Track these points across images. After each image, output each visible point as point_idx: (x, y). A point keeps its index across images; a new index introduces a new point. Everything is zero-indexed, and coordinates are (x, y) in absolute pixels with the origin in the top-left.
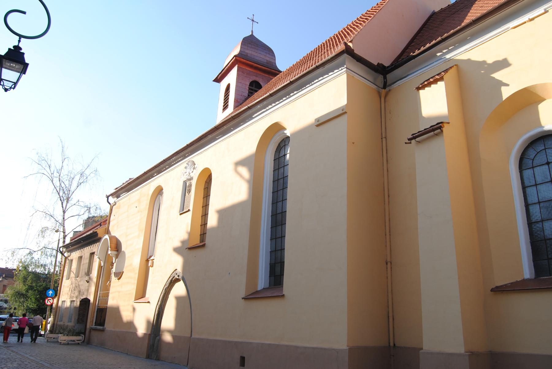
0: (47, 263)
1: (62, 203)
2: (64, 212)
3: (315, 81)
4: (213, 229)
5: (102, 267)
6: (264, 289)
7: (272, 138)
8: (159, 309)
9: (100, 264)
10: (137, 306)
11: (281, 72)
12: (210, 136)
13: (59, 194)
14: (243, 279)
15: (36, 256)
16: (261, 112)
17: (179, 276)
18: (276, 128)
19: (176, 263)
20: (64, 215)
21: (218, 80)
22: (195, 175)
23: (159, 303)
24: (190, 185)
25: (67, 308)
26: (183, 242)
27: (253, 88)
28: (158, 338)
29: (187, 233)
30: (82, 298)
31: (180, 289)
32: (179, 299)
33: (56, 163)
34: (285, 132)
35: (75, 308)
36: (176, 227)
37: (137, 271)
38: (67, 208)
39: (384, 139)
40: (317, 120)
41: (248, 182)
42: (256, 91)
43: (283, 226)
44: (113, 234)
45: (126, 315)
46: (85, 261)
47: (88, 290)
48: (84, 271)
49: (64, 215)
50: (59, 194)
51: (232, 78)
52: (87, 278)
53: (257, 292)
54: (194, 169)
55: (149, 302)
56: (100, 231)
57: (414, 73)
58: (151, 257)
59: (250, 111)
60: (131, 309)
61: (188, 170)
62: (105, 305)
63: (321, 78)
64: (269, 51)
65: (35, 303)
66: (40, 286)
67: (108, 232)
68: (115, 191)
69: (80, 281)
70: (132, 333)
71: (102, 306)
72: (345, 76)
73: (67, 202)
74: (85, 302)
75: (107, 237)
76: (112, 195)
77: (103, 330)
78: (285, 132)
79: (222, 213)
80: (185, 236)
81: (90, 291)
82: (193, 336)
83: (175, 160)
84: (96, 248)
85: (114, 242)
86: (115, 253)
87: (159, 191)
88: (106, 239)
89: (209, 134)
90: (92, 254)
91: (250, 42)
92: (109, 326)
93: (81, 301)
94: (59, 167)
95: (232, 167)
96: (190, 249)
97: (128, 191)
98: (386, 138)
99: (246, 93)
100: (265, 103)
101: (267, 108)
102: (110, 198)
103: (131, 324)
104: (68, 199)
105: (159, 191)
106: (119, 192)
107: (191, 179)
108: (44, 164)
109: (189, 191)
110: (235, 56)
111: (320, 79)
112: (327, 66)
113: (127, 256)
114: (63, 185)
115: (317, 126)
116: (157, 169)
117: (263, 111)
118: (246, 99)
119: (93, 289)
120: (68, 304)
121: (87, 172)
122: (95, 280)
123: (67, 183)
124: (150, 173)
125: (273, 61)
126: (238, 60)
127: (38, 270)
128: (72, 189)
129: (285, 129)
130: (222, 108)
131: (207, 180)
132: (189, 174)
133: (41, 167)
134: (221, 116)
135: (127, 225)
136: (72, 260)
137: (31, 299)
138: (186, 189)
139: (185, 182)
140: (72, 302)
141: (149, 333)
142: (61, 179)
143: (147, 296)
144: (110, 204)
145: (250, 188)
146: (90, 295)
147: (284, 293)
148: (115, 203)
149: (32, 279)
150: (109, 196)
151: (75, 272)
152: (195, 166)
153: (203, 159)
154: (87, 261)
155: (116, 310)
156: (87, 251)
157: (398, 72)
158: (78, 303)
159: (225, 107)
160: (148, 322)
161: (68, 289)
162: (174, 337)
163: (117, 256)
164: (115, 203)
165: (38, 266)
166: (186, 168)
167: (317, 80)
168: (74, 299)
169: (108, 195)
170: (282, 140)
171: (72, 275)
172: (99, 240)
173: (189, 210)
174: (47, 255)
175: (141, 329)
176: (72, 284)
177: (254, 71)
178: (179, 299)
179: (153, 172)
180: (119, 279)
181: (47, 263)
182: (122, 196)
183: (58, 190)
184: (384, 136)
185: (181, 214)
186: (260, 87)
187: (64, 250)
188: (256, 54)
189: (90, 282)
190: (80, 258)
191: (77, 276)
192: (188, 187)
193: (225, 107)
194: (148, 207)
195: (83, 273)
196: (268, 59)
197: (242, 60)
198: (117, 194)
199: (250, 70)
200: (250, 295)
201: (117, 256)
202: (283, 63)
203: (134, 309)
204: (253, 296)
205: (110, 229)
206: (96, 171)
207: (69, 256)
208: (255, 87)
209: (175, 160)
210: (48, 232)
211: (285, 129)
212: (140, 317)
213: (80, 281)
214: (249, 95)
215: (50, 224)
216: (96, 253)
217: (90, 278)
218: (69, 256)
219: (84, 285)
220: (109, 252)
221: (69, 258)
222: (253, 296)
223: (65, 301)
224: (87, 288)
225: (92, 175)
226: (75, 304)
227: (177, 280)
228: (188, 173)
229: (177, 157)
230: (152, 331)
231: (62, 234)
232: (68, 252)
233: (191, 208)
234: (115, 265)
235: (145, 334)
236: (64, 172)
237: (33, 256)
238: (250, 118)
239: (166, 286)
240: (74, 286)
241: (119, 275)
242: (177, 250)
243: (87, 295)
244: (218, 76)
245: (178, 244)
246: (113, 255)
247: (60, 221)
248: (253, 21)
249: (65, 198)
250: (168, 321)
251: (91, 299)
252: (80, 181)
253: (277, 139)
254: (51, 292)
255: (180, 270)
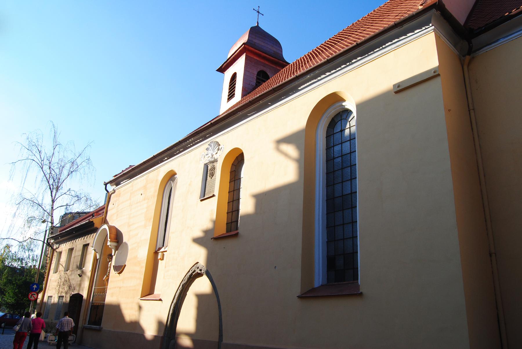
0: (25, 256)
1: (51, 193)
2: (53, 201)
3: (387, 45)
4: (247, 216)
5: (97, 260)
6: (322, 285)
7: (326, 110)
8: (174, 307)
9: (95, 257)
10: (143, 303)
11: (289, 64)
12: (240, 113)
13: (48, 182)
14: (297, 274)
15: (14, 250)
16: (310, 83)
17: (201, 270)
18: (334, 98)
19: (199, 255)
20: (53, 205)
21: (222, 70)
22: (221, 156)
23: (175, 301)
24: (214, 168)
25: (54, 304)
26: (206, 232)
27: (261, 78)
28: (172, 341)
29: (212, 221)
30: (73, 293)
31: (203, 285)
32: (200, 297)
33: (47, 149)
34: (344, 104)
35: (65, 304)
36: (196, 215)
37: (144, 265)
38: (57, 197)
39: (472, 111)
40: (398, 85)
41: (298, 161)
42: (264, 82)
43: (354, 209)
44: (111, 224)
45: (129, 314)
46: (77, 253)
47: (80, 285)
48: (75, 264)
49: (53, 205)
50: (48, 182)
51: (239, 67)
52: (79, 272)
53: (313, 290)
54: (218, 150)
55: (160, 300)
56: (96, 220)
57: (507, 36)
58: (160, 249)
59: (297, 83)
60: (137, 308)
61: (210, 152)
62: (102, 302)
63: (396, 40)
64: (276, 43)
65: (13, 298)
66: (19, 280)
67: (105, 221)
68: (114, 178)
69: (71, 275)
70: (137, 334)
71: (98, 302)
72: (433, 35)
73: (15, 213)
74: (77, 298)
75: (105, 226)
76: (111, 182)
77: (100, 330)
78: (344, 104)
79: (261, 199)
80: (208, 225)
81: (82, 286)
82: (225, 341)
83: (192, 142)
84: (91, 239)
85: (114, 232)
86: (115, 244)
87: (171, 176)
88: (105, 229)
89: (239, 111)
90: (86, 246)
91: (256, 32)
92: (106, 325)
93: (71, 297)
94: (50, 154)
95: (272, 146)
96: (217, 239)
97: (131, 177)
98: (473, 109)
99: (254, 83)
100: (317, 72)
101: (319, 78)
102: (109, 186)
103: (136, 325)
104: (57, 189)
105: (171, 176)
106: (120, 179)
107: (216, 161)
108: (35, 150)
109: (212, 175)
110: (244, 44)
111: (394, 41)
112: (406, 26)
113: (130, 248)
114: (53, 172)
115: (396, 92)
116: (169, 152)
117: (312, 81)
118: (254, 89)
119: (86, 284)
120: (55, 300)
121: (79, 161)
122: (89, 274)
123: (57, 171)
124: (160, 157)
125: (280, 53)
126: (246, 49)
127: (15, 264)
128: (63, 177)
129: (344, 100)
130: (227, 97)
131: (237, 161)
132: (212, 155)
133: (31, 154)
134: (225, 106)
135: (131, 213)
136: (60, 253)
137: (9, 293)
138: (208, 172)
139: (206, 166)
140: (61, 297)
141: (162, 335)
142: (52, 167)
143: (156, 292)
144: (108, 192)
145: (300, 168)
146: (83, 290)
147: (361, 291)
148: (114, 191)
149: (8, 272)
150: (108, 183)
151: (64, 265)
152: (220, 147)
153: (229, 139)
154: (80, 253)
155: (116, 309)
156: (79, 243)
157: (483, 37)
158: (68, 299)
159: (231, 95)
160: (160, 323)
161: (56, 284)
162: (194, 341)
163: (117, 248)
164: (114, 191)
165: (16, 260)
166: (207, 149)
167: (390, 43)
168: (64, 295)
169: (106, 182)
170: (337, 115)
171: (61, 268)
172: (95, 230)
173: (214, 196)
174: (24, 249)
175: (150, 331)
176: (60, 278)
177: (262, 60)
178: (200, 297)
179: (163, 156)
180: (119, 273)
181: (32, 257)
182: (123, 184)
183: (48, 178)
184: (471, 108)
185: (202, 200)
186: (267, 78)
187: (52, 241)
188: (263, 44)
189: (83, 276)
190: (71, 250)
191: (67, 269)
192: (210, 170)
193: (231, 95)
194: (157, 194)
195: (75, 267)
196: (275, 50)
197: (253, 49)
198: (117, 181)
199: (258, 59)
200: (305, 293)
201: (117, 248)
202: (290, 55)
203: (140, 308)
204: (309, 294)
205: (108, 218)
206: (89, 160)
207: (57, 248)
208: (262, 77)
209: (192, 142)
210: (34, 223)
211: (344, 100)
212: (150, 319)
213: (71, 275)
214: (256, 85)
215: (37, 213)
216: (91, 245)
217: (83, 272)
218: (57, 248)
219: (75, 279)
220: (109, 243)
221: (57, 250)
222: (309, 294)
223: (51, 296)
224: (79, 283)
225: (84, 164)
226: (64, 300)
227: (199, 275)
228: (210, 155)
229: (195, 138)
230: (165, 333)
231: (50, 225)
232: (57, 243)
233: (216, 193)
234: (114, 258)
235: (155, 336)
236: (55, 160)
237: (11, 249)
238: (295, 90)
239: (184, 282)
240: (63, 280)
241: (120, 269)
242: (197, 241)
243: (79, 291)
244: (223, 65)
245: (199, 234)
246: (112, 247)
247: (48, 211)
248: (258, 12)
249: (55, 186)
250: (187, 322)
251: (85, 295)
252: (72, 170)
253: (332, 112)
254: (35, 286)
255: (202, 261)
